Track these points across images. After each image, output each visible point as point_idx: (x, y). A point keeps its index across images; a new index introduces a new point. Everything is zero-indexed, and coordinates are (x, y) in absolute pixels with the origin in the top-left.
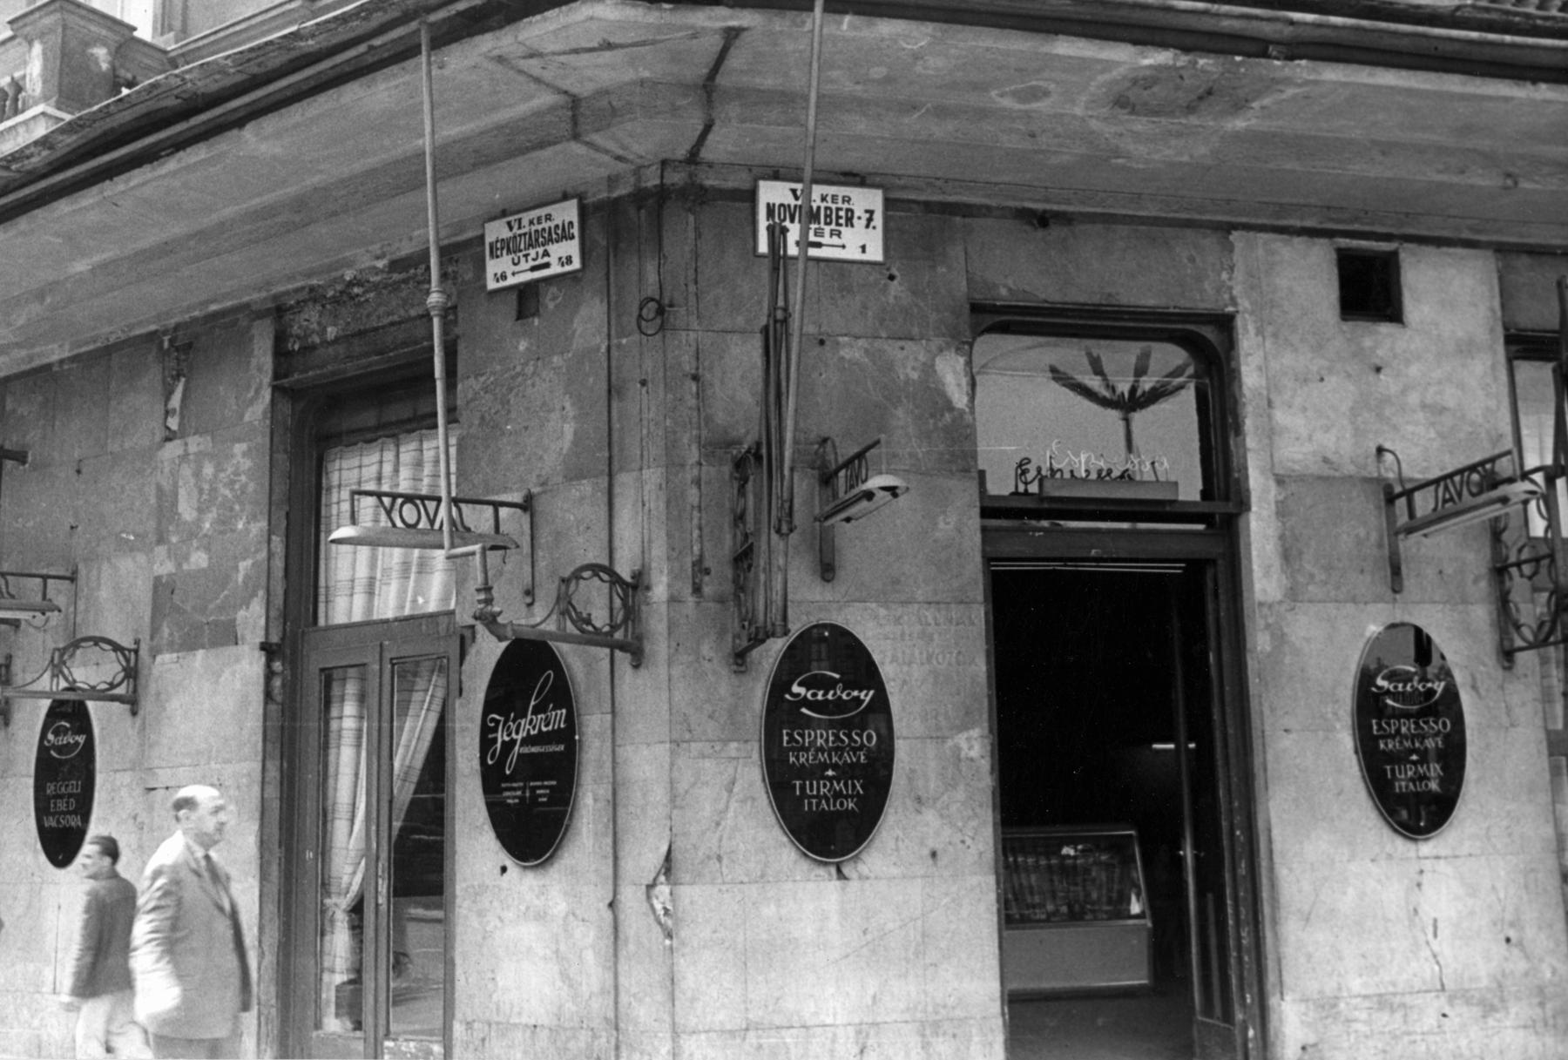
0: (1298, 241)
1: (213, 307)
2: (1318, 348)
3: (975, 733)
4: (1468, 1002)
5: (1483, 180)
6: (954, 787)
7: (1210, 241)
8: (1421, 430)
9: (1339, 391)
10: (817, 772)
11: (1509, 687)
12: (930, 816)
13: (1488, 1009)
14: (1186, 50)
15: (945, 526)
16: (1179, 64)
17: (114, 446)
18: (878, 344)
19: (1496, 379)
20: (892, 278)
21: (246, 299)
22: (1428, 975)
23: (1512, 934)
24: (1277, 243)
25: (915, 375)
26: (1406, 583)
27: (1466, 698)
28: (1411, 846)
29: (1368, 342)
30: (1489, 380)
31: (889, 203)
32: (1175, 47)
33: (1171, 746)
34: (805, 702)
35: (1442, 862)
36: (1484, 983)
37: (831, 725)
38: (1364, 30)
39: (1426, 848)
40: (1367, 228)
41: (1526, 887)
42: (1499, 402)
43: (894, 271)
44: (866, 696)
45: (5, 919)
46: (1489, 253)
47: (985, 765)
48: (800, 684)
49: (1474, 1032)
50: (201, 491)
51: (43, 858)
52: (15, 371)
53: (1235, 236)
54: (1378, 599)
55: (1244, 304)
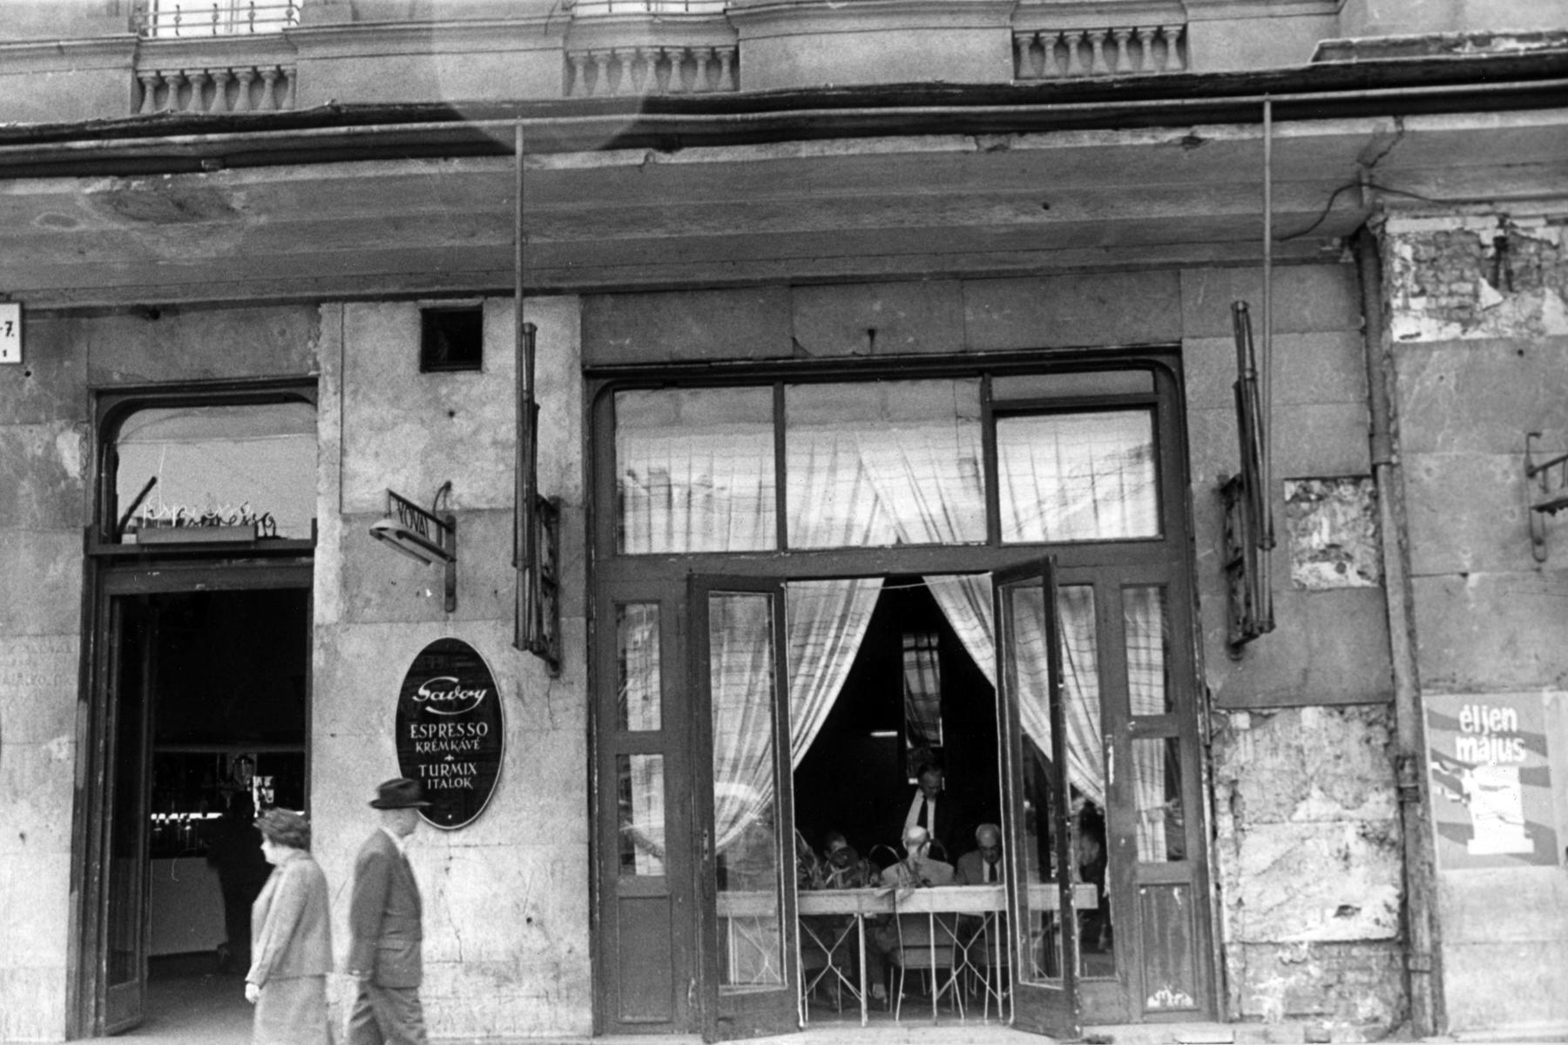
0: (384, 307)
2: (396, 400)
3: (65, 739)
4: (483, 973)
5: (490, 239)
6: (45, 781)
7: (299, 318)
8: (488, 465)
9: (412, 437)
10: (437, 758)
11: (555, 694)
12: (24, 806)
13: (503, 979)
14: (122, 175)
15: (55, 571)
16: (116, 188)
18: (13, 429)
19: (569, 413)
20: (28, 374)
22: (448, 949)
23: (533, 914)
24: (363, 309)
25: (40, 452)
26: (460, 602)
27: (509, 706)
28: (445, 836)
29: (444, 391)
30: (562, 413)
31: (24, 313)
32: (114, 174)
33: (894, 734)
34: (429, 702)
35: (471, 850)
36: (503, 957)
37: (456, 720)
38: (240, 140)
39: (457, 838)
40: (448, 288)
41: (553, 874)
42: (571, 434)
43: (30, 369)
44: (479, 695)
46: (575, 298)
47: (70, 764)
49: (487, 997)
53: (324, 308)
54: (433, 618)
55: (326, 367)
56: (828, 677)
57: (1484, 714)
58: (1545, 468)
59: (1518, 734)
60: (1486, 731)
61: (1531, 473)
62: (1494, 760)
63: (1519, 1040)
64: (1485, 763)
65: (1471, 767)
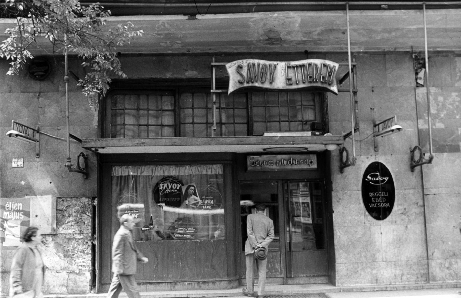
1: (439, 49)
17: (389, 85)
21: (453, 49)
34: (371, 181)
44: (386, 179)
45: (459, 232)
48: (370, 176)
50: (438, 105)
51: (370, 218)
52: (332, 51)
56: (119, 185)
57: (13, 205)
58: (378, 124)
59: (22, 211)
60: (13, 210)
61: (375, 126)
62: (14, 219)
63: (220, 297)
64: (11, 219)
65: (7, 220)
